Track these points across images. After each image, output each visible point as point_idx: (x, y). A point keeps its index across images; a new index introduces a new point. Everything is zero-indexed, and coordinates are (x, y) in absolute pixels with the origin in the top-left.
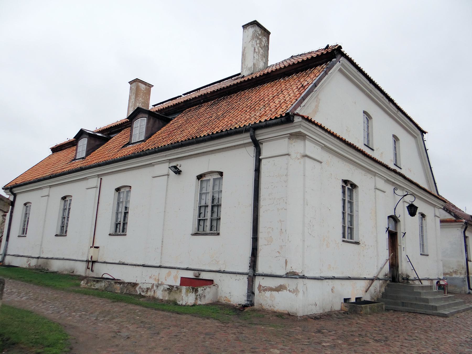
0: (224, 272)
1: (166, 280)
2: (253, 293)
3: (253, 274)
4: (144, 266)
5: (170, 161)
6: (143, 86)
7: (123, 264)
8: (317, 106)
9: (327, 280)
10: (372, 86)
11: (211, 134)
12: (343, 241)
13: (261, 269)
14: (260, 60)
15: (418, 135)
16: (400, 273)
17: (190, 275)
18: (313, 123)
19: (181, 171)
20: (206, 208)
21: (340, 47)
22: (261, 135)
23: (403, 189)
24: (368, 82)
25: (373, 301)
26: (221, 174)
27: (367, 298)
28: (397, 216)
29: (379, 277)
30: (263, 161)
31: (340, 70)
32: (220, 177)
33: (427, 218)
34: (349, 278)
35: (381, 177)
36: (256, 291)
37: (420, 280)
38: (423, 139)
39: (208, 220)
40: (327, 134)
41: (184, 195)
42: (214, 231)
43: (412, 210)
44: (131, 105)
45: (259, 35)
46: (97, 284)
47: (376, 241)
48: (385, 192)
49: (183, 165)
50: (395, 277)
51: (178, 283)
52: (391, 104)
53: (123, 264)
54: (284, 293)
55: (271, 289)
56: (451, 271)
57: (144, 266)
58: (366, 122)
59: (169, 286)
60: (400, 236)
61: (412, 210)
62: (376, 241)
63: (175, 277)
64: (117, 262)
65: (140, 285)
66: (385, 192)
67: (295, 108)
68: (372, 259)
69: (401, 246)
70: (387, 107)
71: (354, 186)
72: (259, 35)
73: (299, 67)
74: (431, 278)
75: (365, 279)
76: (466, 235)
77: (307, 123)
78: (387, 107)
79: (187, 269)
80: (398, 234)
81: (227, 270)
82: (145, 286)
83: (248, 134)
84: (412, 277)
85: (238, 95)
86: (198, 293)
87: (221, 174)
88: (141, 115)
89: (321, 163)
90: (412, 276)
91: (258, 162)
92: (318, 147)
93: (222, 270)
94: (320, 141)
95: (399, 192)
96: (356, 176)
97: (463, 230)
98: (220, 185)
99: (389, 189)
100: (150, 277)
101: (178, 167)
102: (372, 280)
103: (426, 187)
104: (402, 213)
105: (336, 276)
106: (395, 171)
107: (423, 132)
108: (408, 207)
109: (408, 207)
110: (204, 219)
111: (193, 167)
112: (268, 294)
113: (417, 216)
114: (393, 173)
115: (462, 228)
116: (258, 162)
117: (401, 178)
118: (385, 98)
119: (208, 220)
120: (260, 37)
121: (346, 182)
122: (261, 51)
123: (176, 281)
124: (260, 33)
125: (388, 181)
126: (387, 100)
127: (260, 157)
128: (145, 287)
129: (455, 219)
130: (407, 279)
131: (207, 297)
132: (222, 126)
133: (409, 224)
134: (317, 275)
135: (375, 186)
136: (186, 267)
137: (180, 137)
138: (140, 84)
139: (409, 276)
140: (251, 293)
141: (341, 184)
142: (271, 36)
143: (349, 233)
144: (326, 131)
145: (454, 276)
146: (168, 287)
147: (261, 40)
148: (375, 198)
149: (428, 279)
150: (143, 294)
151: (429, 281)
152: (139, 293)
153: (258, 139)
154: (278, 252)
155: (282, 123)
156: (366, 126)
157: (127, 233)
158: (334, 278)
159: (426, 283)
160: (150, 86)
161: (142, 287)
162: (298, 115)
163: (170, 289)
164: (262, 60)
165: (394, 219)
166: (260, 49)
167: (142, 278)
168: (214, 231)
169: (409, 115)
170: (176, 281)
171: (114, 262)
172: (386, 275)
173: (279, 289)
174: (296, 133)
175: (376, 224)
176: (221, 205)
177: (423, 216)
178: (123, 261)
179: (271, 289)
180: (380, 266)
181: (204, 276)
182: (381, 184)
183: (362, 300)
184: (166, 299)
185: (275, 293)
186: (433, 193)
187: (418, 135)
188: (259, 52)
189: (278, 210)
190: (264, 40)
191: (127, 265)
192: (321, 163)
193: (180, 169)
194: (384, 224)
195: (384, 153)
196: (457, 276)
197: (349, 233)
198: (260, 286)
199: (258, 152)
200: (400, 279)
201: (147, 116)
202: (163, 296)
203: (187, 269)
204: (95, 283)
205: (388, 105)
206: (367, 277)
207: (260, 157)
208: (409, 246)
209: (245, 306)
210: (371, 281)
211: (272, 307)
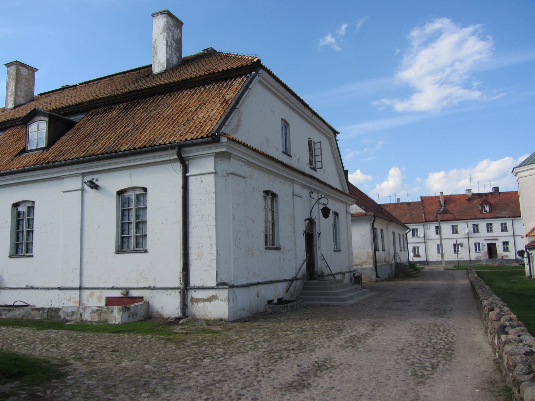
0: (154, 288)
1: (88, 301)
2: (187, 306)
3: (186, 287)
4: (60, 288)
5: (84, 175)
6: (24, 71)
7: (32, 288)
8: (239, 121)
9: (253, 287)
10: (288, 94)
11: (132, 148)
12: (266, 248)
13: (193, 282)
14: (173, 55)
15: (331, 136)
16: (316, 270)
17: (117, 294)
18: (238, 142)
19: (98, 186)
20: (130, 225)
21: (259, 61)
22: (188, 153)
23: (318, 192)
24: (285, 91)
25: (293, 299)
26: (145, 189)
27: (287, 297)
28: (314, 218)
29: (297, 277)
30: (191, 179)
31: (260, 82)
32: (143, 192)
33: (340, 216)
34: (272, 282)
35: (298, 183)
36: (189, 304)
37: (333, 275)
38: (336, 139)
39: (131, 235)
40: (249, 150)
41: (103, 210)
42: (140, 246)
43: (326, 212)
44: (10, 93)
45: (171, 27)
46: (10, 313)
47: (295, 244)
48: (301, 197)
49: (102, 180)
50: (311, 271)
51: (103, 303)
52: (307, 109)
53: (32, 288)
54: (216, 302)
55: (204, 300)
56: (362, 261)
57: (60, 288)
58: (284, 129)
59: (99, 307)
60: (316, 236)
61: (326, 212)
62: (295, 244)
63: (100, 298)
64: (24, 286)
65: (64, 309)
66: (301, 197)
67: (220, 128)
68: (290, 260)
69: (316, 246)
70: (303, 112)
71: (274, 195)
72: (171, 27)
73: (219, 76)
74: (343, 271)
75: (285, 280)
76: (375, 226)
77: (232, 142)
78: (303, 112)
79: (113, 288)
80: (314, 235)
81: (158, 285)
82: (69, 310)
83: (175, 151)
84: (326, 273)
85: (154, 100)
86: (130, 312)
87: (145, 189)
88: (38, 118)
89: (245, 178)
90: (326, 272)
91: (185, 180)
92: (241, 163)
93: (152, 286)
94: (243, 157)
95: (315, 195)
96: (277, 186)
97: (372, 222)
98: (145, 201)
99: (305, 193)
100: (69, 300)
101: (94, 181)
102: (292, 281)
103: (340, 188)
104: (317, 215)
105: (260, 281)
106: (311, 177)
107: (336, 133)
108: (322, 210)
109: (322, 210)
110: (128, 237)
111: (114, 182)
112: (200, 305)
113: (331, 215)
114: (309, 178)
115: (370, 220)
116: (185, 180)
117: (316, 181)
118: (300, 104)
119: (131, 235)
120: (173, 29)
121: (267, 192)
122: (174, 44)
123: (100, 302)
124: (172, 24)
125: (304, 186)
126: (303, 106)
127: (187, 174)
128: (70, 311)
129: (364, 212)
130: (322, 275)
131: (139, 314)
132: (143, 138)
133: (324, 226)
134: (244, 283)
135: (293, 192)
136: (111, 286)
137: (96, 149)
138: (21, 67)
139: (323, 273)
140: (184, 306)
141: (262, 194)
142: (184, 27)
143: (271, 243)
144: (249, 148)
145: (364, 266)
146: (97, 309)
147: (173, 32)
148: (293, 204)
149: (340, 273)
150: (67, 318)
151: (342, 275)
152: (63, 317)
153: (183, 156)
154: (209, 266)
155: (208, 143)
156: (284, 132)
157: (34, 253)
158: (258, 284)
159: (338, 277)
160: (33, 70)
161: (66, 311)
162: (224, 134)
163: (99, 311)
164: (175, 54)
165: (311, 222)
166: (173, 42)
167: (65, 302)
168: (140, 246)
169: (323, 118)
170: (100, 302)
171: (19, 286)
172: (304, 275)
173: (211, 299)
174: (222, 152)
175: (294, 228)
176: (146, 222)
177: (336, 214)
178: (31, 285)
179: (204, 300)
180: (298, 267)
181: (134, 294)
182: (298, 189)
183: (284, 300)
184: (96, 320)
185: (207, 304)
186: (346, 192)
187: (331, 136)
188: (172, 46)
189: (207, 226)
190: (176, 32)
191: (37, 289)
192: (245, 178)
193: (97, 183)
194: (302, 226)
195: (300, 159)
196: (367, 266)
197: (271, 243)
198: (192, 298)
199: (185, 170)
200: (316, 276)
201: (47, 119)
202: (92, 318)
203: (113, 288)
204: (6, 312)
205: (304, 110)
206: (287, 278)
207: (187, 174)
208: (324, 246)
209: (179, 319)
210: (291, 282)
211: (205, 317)
